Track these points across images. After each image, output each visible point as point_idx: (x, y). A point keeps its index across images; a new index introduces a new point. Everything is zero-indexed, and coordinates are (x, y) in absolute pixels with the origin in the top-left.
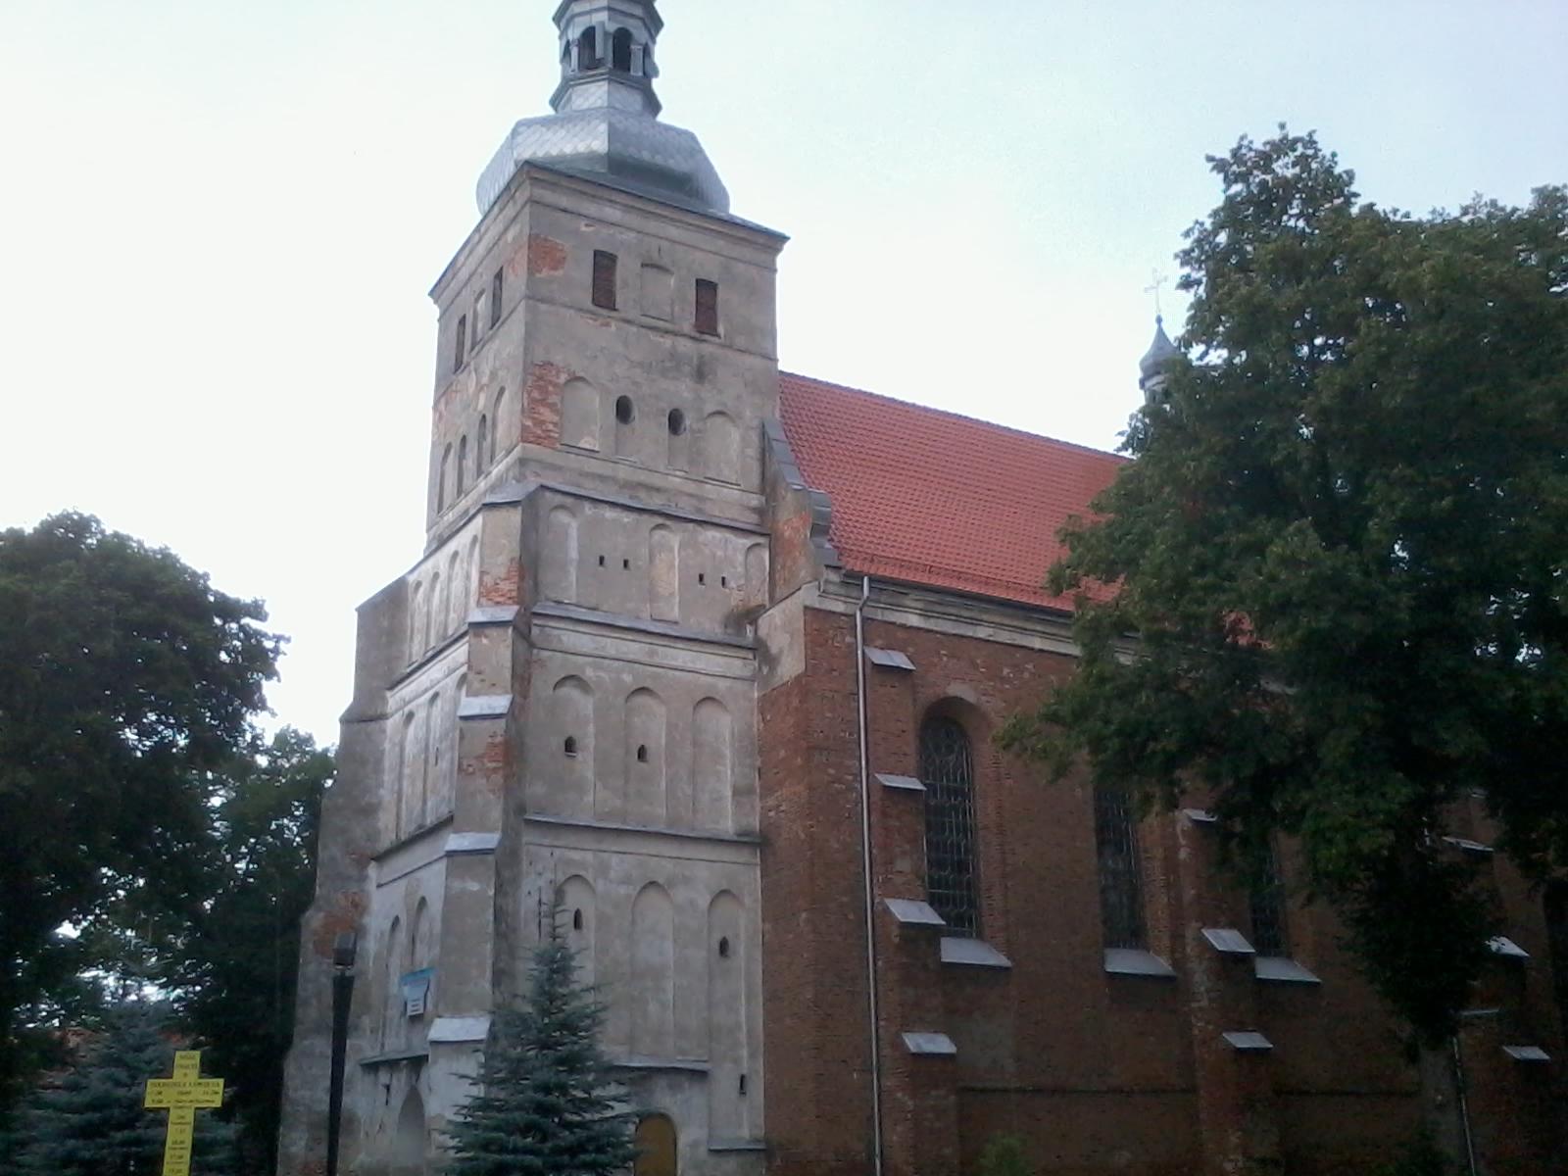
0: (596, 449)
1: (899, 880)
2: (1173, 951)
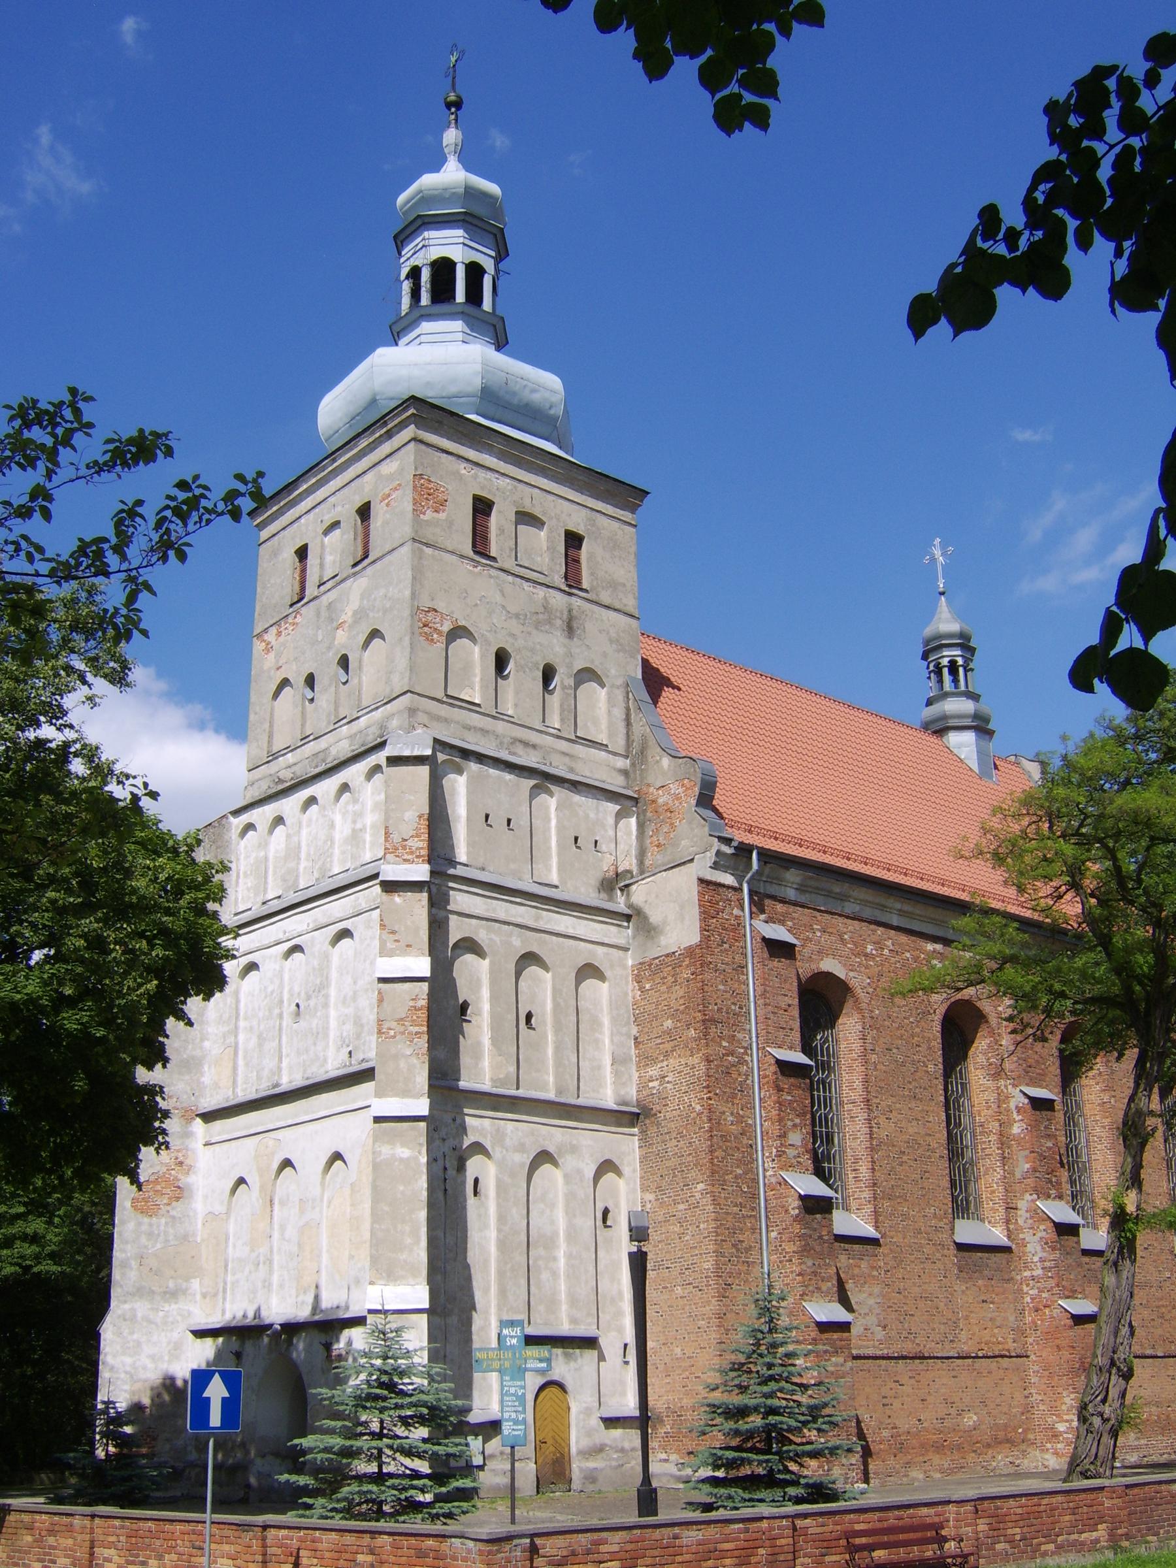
0: (477, 701)
1: (791, 1152)
2: (1008, 1222)
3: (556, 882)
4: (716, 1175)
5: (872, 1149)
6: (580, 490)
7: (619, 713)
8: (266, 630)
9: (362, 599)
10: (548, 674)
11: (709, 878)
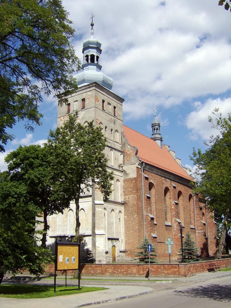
2: (171, 222)
3: (113, 165)
4: (138, 214)
5: (156, 210)
6: (118, 100)
7: (120, 137)
8: (61, 117)
9: (83, 115)
10: (112, 130)
11: (138, 167)
